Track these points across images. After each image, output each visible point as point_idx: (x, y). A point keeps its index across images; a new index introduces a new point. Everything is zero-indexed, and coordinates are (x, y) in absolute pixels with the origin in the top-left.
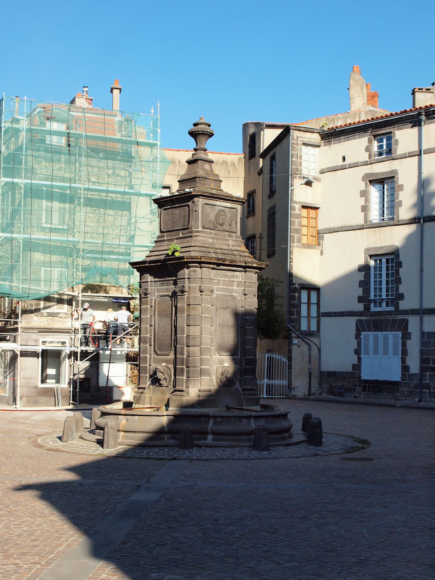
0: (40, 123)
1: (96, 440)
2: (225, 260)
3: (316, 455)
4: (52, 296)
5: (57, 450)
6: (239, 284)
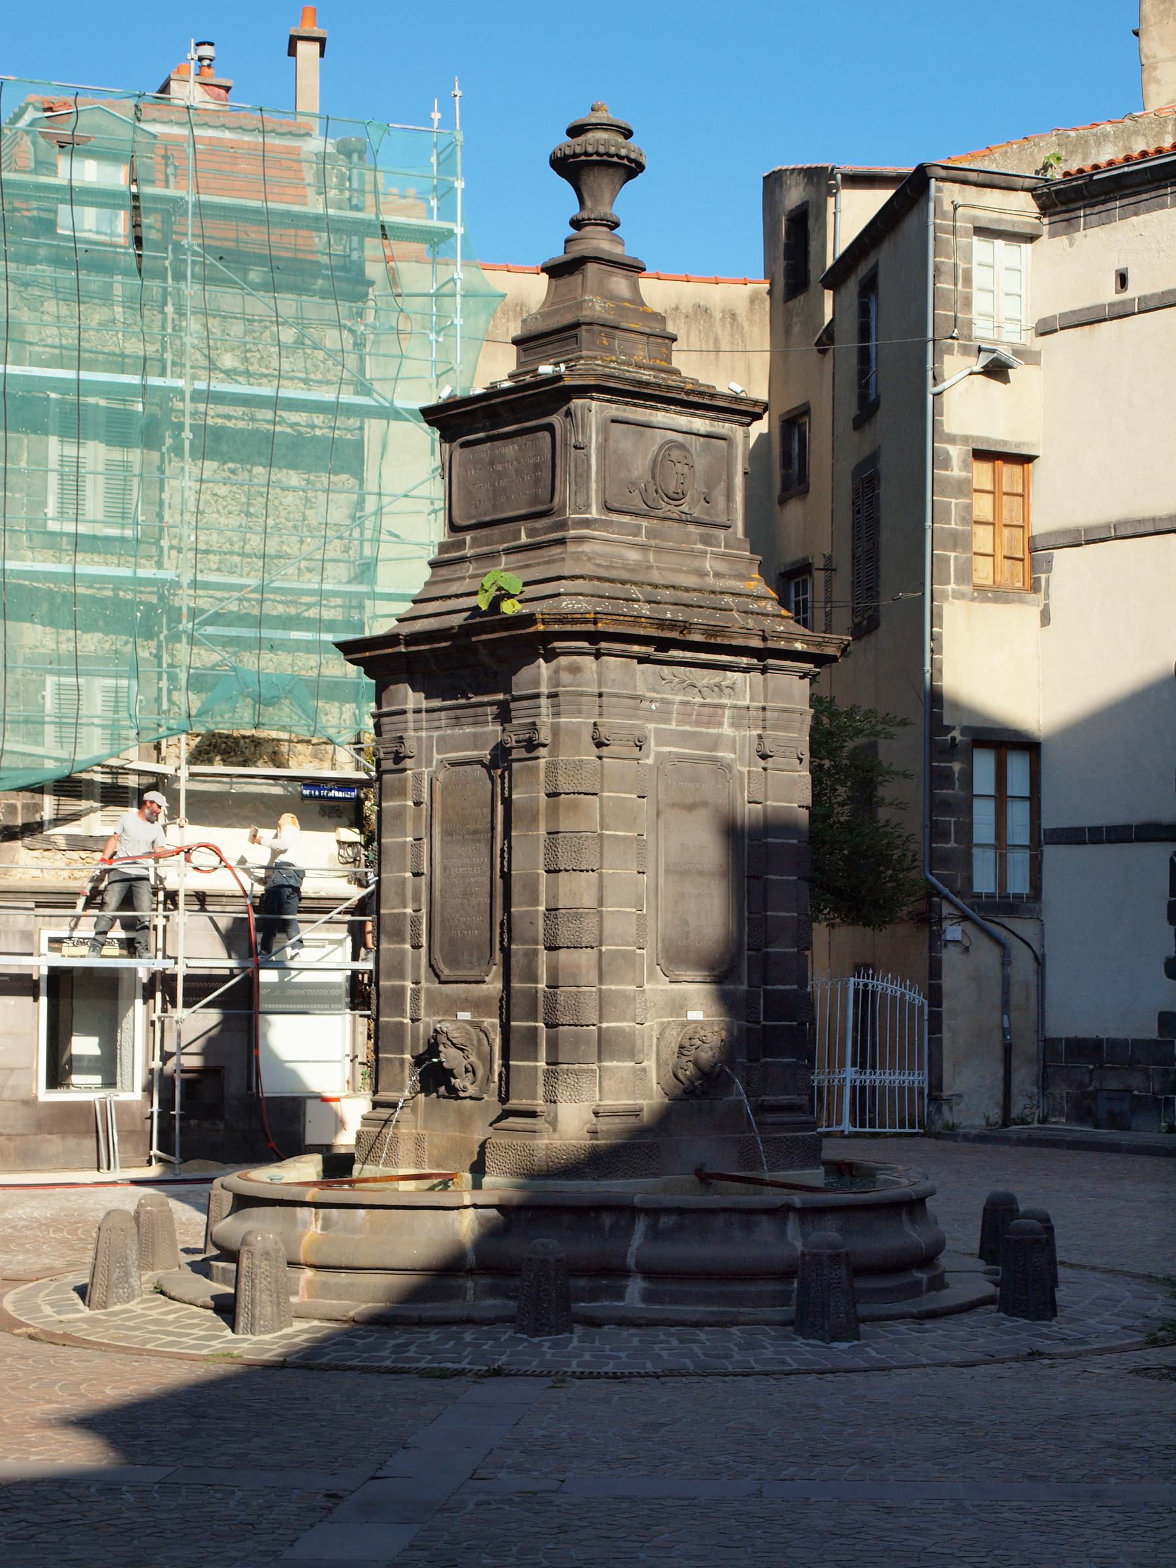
0: (37, 162)
1: (213, 1298)
2: (686, 627)
3: (1035, 1355)
4: (85, 776)
5: (65, 1340)
6: (741, 718)
